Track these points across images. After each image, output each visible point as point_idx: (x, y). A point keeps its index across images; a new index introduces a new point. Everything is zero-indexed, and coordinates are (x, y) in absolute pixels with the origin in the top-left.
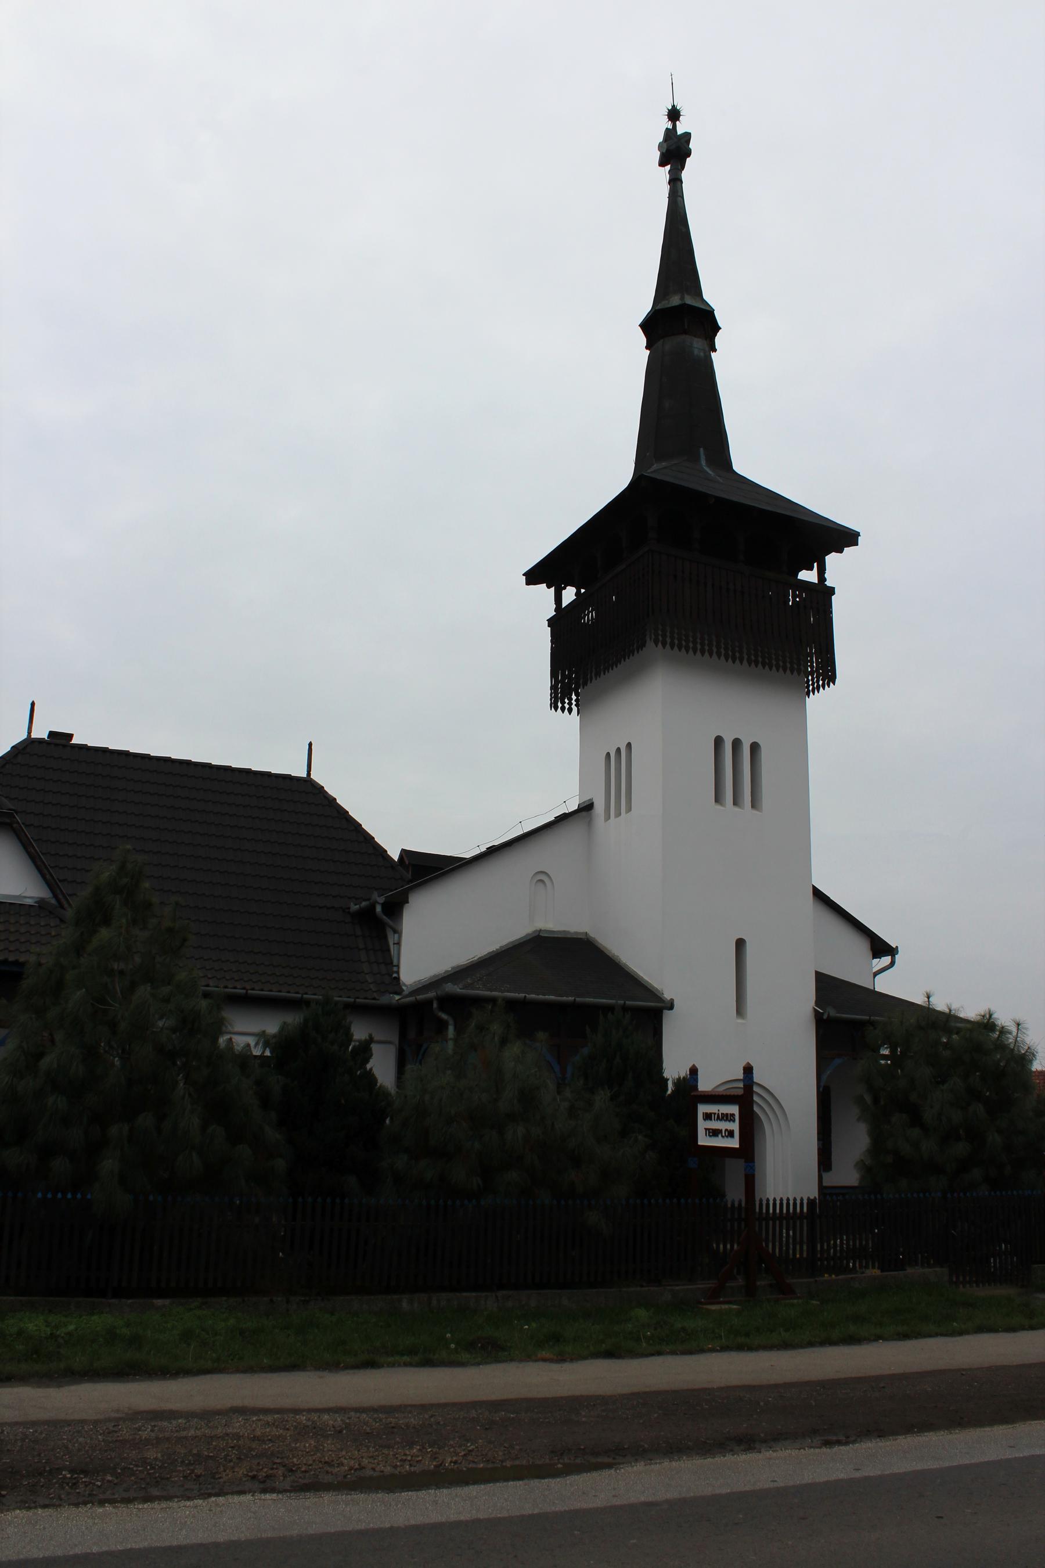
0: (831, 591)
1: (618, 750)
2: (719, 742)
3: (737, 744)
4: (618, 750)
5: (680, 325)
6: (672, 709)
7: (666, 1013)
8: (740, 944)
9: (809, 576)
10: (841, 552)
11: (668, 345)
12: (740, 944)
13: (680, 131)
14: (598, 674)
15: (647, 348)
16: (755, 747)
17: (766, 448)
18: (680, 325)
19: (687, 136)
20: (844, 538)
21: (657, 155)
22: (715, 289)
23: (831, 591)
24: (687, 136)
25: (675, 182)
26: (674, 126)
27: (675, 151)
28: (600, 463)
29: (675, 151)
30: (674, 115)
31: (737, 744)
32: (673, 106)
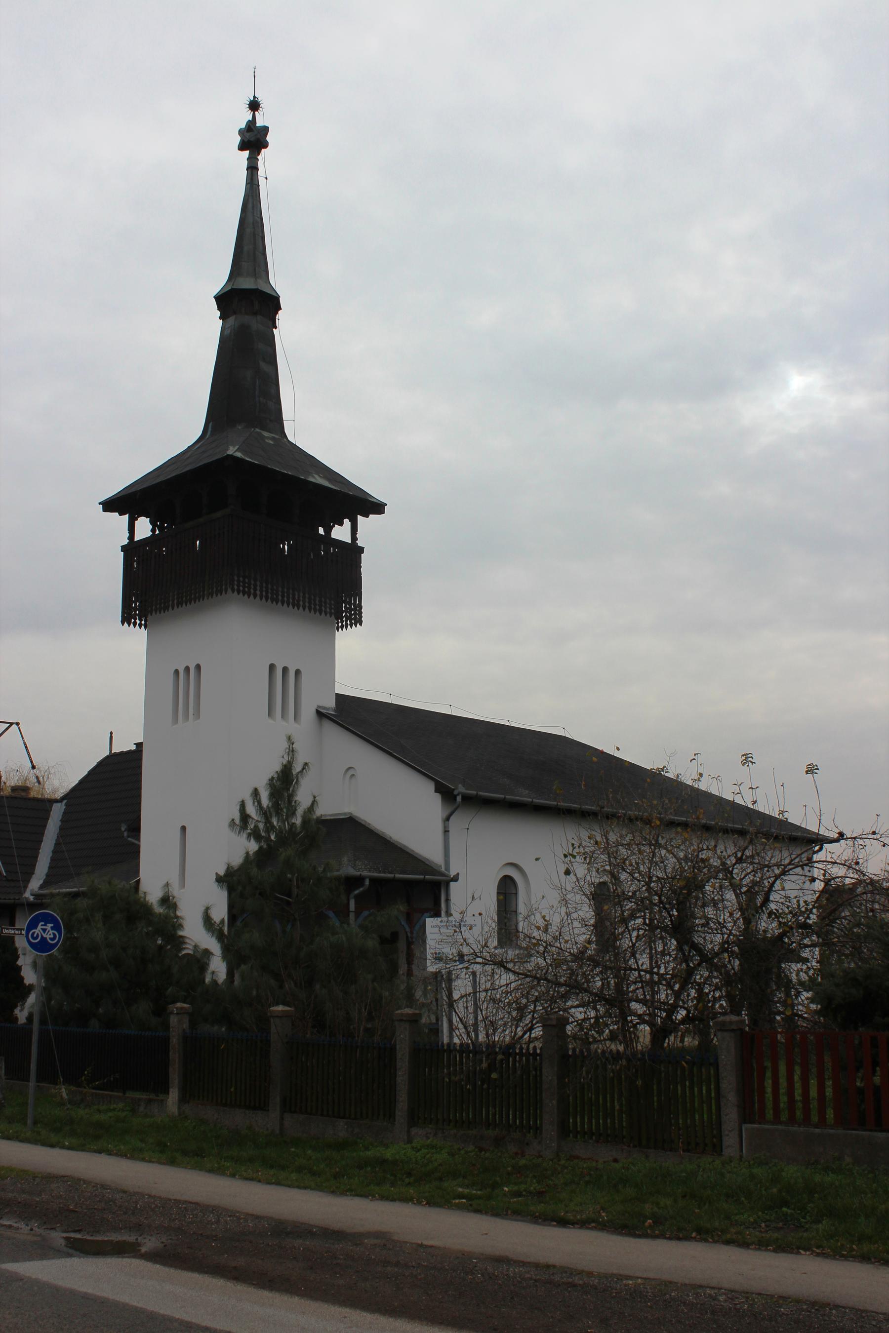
0: (361, 550)
1: (187, 669)
2: (272, 667)
3: (285, 670)
4: (187, 669)
5: (249, 306)
6: (238, 638)
7: (452, 884)
8: (184, 829)
9: (341, 533)
10: (368, 517)
11: (231, 320)
12: (184, 829)
13: (259, 123)
14: (180, 604)
15: (220, 318)
16: (298, 672)
17: (318, 421)
18: (249, 306)
19: (265, 130)
20: (377, 508)
21: (238, 139)
22: (280, 279)
23: (361, 550)
24: (265, 130)
25: (252, 168)
26: (254, 116)
27: (254, 140)
28: (172, 419)
29: (254, 140)
30: (254, 106)
31: (285, 670)
32: (255, 97)
